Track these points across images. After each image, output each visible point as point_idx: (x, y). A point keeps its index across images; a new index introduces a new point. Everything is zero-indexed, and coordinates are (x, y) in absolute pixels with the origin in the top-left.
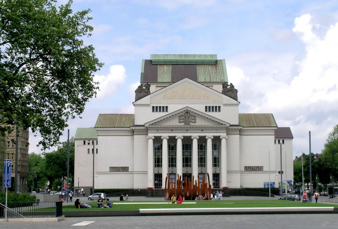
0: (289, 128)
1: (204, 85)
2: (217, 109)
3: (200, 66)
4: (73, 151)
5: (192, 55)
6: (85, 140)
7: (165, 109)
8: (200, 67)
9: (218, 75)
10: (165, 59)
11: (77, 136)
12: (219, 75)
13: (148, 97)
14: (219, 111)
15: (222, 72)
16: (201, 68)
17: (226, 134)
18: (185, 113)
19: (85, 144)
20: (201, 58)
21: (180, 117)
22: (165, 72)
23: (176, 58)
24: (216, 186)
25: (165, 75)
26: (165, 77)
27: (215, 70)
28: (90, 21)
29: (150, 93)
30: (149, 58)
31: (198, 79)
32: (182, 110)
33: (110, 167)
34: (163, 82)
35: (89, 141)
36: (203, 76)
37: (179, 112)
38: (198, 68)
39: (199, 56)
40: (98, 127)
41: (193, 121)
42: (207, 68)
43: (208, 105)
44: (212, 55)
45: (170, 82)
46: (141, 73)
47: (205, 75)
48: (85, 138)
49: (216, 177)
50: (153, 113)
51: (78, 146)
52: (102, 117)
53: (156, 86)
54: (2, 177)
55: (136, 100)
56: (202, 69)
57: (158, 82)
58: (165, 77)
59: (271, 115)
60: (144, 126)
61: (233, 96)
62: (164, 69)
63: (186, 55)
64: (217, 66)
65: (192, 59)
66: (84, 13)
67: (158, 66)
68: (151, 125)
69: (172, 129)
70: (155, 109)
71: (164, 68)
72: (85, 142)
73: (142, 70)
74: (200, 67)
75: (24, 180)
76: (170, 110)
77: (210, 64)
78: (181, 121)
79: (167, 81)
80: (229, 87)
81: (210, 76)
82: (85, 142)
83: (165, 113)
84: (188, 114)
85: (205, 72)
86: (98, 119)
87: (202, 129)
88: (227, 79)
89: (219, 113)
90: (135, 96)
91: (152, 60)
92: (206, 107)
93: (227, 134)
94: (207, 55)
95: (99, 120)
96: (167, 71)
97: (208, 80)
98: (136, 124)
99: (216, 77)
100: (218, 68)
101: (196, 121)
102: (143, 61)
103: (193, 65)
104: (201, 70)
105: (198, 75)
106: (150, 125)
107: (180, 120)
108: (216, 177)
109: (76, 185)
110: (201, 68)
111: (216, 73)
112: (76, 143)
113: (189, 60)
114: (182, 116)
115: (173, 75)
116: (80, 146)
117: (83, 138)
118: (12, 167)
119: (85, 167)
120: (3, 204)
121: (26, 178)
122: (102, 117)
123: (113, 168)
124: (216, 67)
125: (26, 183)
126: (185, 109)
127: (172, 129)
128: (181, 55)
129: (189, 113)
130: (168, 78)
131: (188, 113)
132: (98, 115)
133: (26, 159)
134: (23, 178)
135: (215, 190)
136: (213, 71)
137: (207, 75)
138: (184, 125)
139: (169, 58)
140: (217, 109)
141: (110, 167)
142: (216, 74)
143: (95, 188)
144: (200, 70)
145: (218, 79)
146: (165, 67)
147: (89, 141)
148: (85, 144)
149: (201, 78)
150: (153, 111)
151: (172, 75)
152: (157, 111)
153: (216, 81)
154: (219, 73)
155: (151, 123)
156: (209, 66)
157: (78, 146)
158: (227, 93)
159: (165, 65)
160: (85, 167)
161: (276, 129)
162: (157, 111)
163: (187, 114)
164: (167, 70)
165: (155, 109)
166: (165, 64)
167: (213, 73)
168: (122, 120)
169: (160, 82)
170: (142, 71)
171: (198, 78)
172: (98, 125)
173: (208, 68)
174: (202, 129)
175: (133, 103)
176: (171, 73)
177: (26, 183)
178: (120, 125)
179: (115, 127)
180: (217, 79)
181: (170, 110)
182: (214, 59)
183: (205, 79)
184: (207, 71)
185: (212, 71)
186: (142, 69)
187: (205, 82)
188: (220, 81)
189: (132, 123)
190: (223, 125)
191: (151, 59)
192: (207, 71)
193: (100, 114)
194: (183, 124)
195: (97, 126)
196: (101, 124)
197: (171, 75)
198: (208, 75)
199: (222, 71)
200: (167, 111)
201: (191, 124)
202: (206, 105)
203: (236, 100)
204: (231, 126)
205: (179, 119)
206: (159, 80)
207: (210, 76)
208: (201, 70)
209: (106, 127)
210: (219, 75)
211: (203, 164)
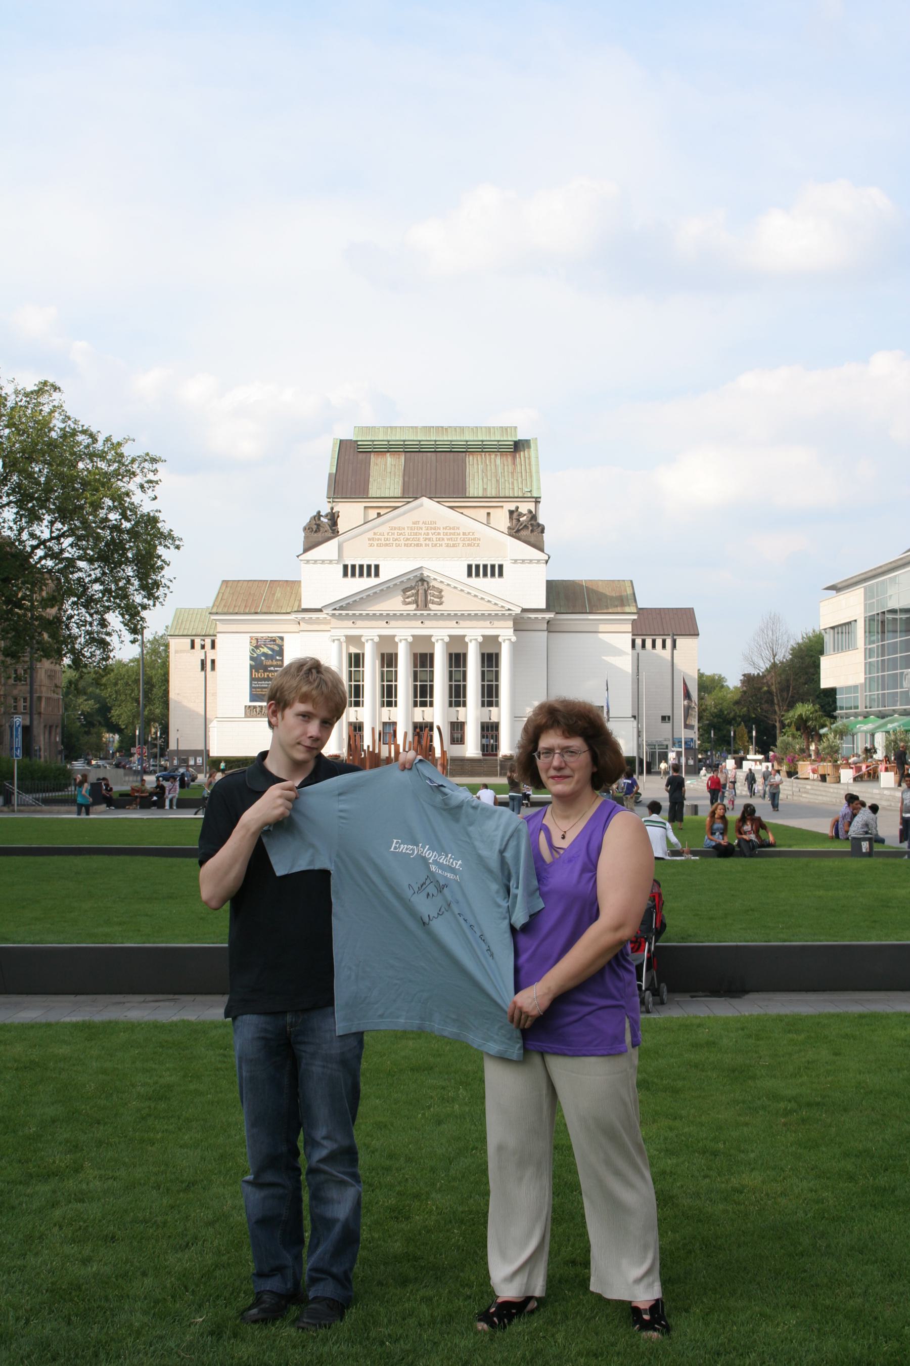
0: (693, 609)
1: (465, 511)
2: (497, 571)
3: (475, 455)
4: (165, 665)
5: (455, 428)
6: (193, 638)
7: (373, 570)
8: (475, 459)
9: (517, 480)
10: (389, 438)
11: (176, 628)
12: (520, 480)
13: (333, 544)
14: (501, 574)
15: (528, 471)
16: (477, 460)
17: (512, 630)
18: (417, 582)
19: (193, 647)
20: (477, 436)
21: (405, 591)
22: (389, 470)
23: (417, 435)
24: (492, 751)
25: (388, 480)
26: (388, 484)
27: (510, 467)
28: (117, 637)
29: (338, 532)
30: (349, 435)
31: (467, 490)
32: (411, 576)
33: (246, 706)
34: (383, 495)
35: (204, 640)
36: (481, 481)
37: (404, 579)
38: (470, 459)
39: (473, 429)
40: (217, 613)
41: (436, 600)
42: (493, 460)
43: (474, 563)
44: (506, 428)
45: (400, 496)
46: (330, 475)
47: (485, 480)
48: (194, 634)
49: (492, 730)
50: (346, 579)
51: (176, 652)
52: (229, 589)
53: (365, 507)
54: (677, 824)
55: (306, 550)
56: (480, 463)
57: (370, 496)
58: (388, 484)
59: (628, 584)
60: (320, 610)
61: (532, 540)
62: (386, 465)
63: (442, 427)
64: (517, 456)
65: (454, 438)
66: (154, 460)
67: (372, 455)
68: (338, 610)
69: (388, 618)
70: (349, 571)
71: (386, 460)
72: (193, 642)
73: (331, 465)
74: (475, 459)
75: (53, 733)
76: (385, 575)
77: (498, 452)
78: (407, 600)
79: (392, 495)
80: (525, 518)
81: (498, 481)
82: (193, 642)
83: (372, 581)
84: (425, 584)
85: (484, 471)
86: (219, 593)
87: (458, 617)
88: (539, 488)
89: (500, 579)
90: (303, 539)
91: (357, 441)
92: (470, 567)
93: (514, 630)
94: (494, 427)
95: (221, 595)
96: (393, 470)
97: (491, 492)
98: (304, 606)
99: (513, 484)
100: (518, 459)
101: (443, 599)
102: (334, 444)
103: (456, 454)
104: (475, 466)
105: (467, 480)
106: (335, 609)
107: (404, 598)
108: (492, 730)
109: (172, 746)
110: (477, 460)
111: (512, 473)
112: (174, 643)
113: (448, 441)
114: (411, 588)
115: (406, 479)
116: (182, 651)
117: (189, 634)
118: (24, 702)
119: (195, 702)
120: (11, 784)
121: (57, 727)
122: (229, 589)
123: (252, 708)
124: (514, 458)
125: (58, 739)
126: (418, 573)
127: (388, 618)
128: (427, 429)
129: (428, 583)
130: (394, 486)
131: (424, 581)
132: (220, 583)
133: (35, 662)
134: (51, 727)
135: (485, 760)
136: (506, 467)
137: (491, 480)
138: (415, 610)
139: (398, 437)
140: (497, 571)
141: (246, 706)
142: (513, 477)
143: (211, 755)
144: (475, 467)
145: (516, 489)
146: (389, 459)
147: (204, 640)
148: (193, 647)
149: (476, 486)
150: (345, 574)
151: (404, 480)
152: (353, 575)
153: (511, 495)
154: (519, 475)
155: (337, 606)
156: (496, 455)
157: (176, 652)
158: (524, 533)
159: (388, 454)
160: (195, 702)
161: (634, 620)
162: (353, 575)
163: (423, 585)
164: (393, 467)
165: (349, 571)
166: (388, 452)
167: (506, 473)
168: (274, 594)
169: (373, 498)
170: (331, 469)
171: (467, 486)
172: (218, 607)
173: (495, 461)
174: (458, 617)
175: (298, 556)
176: (401, 474)
177: (58, 739)
178: (269, 607)
179: (256, 613)
180: (513, 489)
181: (385, 575)
182: (510, 439)
183: (485, 490)
184: (491, 470)
185: (504, 469)
186: (331, 463)
187: (485, 495)
188: (521, 495)
189: (297, 604)
190: (507, 610)
191: (355, 439)
192: (491, 470)
193: (225, 582)
194: (414, 606)
195: (214, 610)
196: (225, 606)
197: (401, 479)
198: (494, 480)
199: (527, 467)
200: (377, 575)
201: (431, 606)
202: (470, 563)
203: (542, 550)
204: (524, 610)
205: (402, 596)
206: (373, 492)
207: (498, 481)
208: (475, 466)
209: (237, 613)
210: (520, 480)
211: (428, 699)
